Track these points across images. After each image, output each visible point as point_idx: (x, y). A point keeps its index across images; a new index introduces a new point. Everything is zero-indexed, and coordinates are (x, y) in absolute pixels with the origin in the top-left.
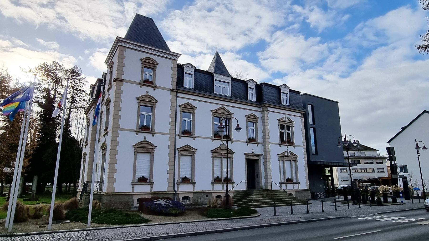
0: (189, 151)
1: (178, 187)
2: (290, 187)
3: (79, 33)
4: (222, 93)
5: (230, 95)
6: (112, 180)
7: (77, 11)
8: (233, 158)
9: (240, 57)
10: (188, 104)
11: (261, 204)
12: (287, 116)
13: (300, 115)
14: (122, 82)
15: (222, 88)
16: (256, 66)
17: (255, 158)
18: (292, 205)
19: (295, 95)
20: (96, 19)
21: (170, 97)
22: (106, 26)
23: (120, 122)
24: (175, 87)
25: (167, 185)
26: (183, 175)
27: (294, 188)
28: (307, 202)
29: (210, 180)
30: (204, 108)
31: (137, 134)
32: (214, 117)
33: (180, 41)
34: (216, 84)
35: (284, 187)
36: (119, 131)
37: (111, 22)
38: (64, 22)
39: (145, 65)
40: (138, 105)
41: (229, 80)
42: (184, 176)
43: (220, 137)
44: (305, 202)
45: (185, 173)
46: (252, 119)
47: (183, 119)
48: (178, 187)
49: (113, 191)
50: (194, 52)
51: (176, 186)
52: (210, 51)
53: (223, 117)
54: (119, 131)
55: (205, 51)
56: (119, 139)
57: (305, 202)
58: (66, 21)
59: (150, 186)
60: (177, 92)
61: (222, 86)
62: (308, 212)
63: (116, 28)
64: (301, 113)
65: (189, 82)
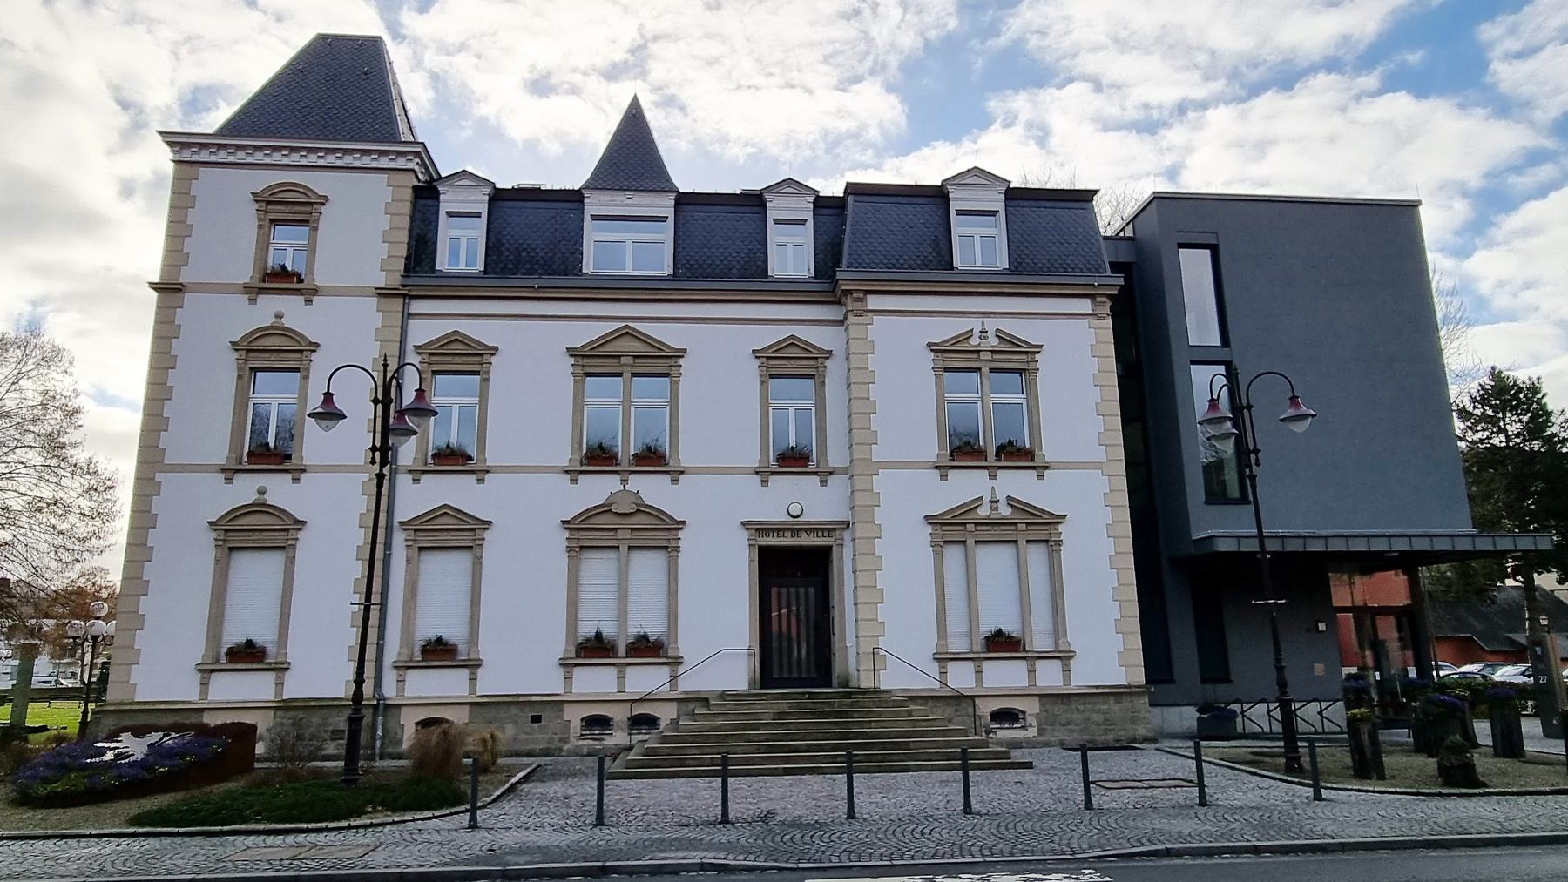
0: (456, 532)
1: (401, 681)
2: (1004, 675)
3: (724, 140)
4: (629, 270)
5: (1002, 262)
7: (712, 62)
8: (1059, 543)
9: (1370, 81)
10: (456, 338)
11: (681, 763)
12: (992, 325)
13: (1085, 306)
14: (179, 295)
15: (977, 238)
16: (1462, 106)
17: (805, 540)
18: (725, 776)
19: (1047, 213)
20: (771, 74)
21: (377, 319)
22: (810, 92)
24: (396, 280)
26: (427, 630)
27: (979, 680)
28: (725, 762)
29: (558, 645)
30: (532, 346)
31: (574, 481)
32: (947, 370)
33: (1085, 78)
34: (959, 227)
35: (961, 678)
36: (159, 477)
37: (824, 68)
38: (676, 111)
39: (272, 216)
40: (239, 369)
41: (664, 206)
42: (432, 636)
43: (980, 453)
44: (712, 762)
45: (440, 618)
46: (788, 363)
48: (401, 681)
49: (126, 698)
50: (1146, 106)
51: (390, 677)
52: (1218, 86)
54: (159, 477)
55: (1199, 93)
57: (712, 762)
58: (683, 109)
59: (465, 673)
60: (404, 296)
61: (629, 237)
63: (842, 87)
64: (1092, 297)
65: (461, 245)
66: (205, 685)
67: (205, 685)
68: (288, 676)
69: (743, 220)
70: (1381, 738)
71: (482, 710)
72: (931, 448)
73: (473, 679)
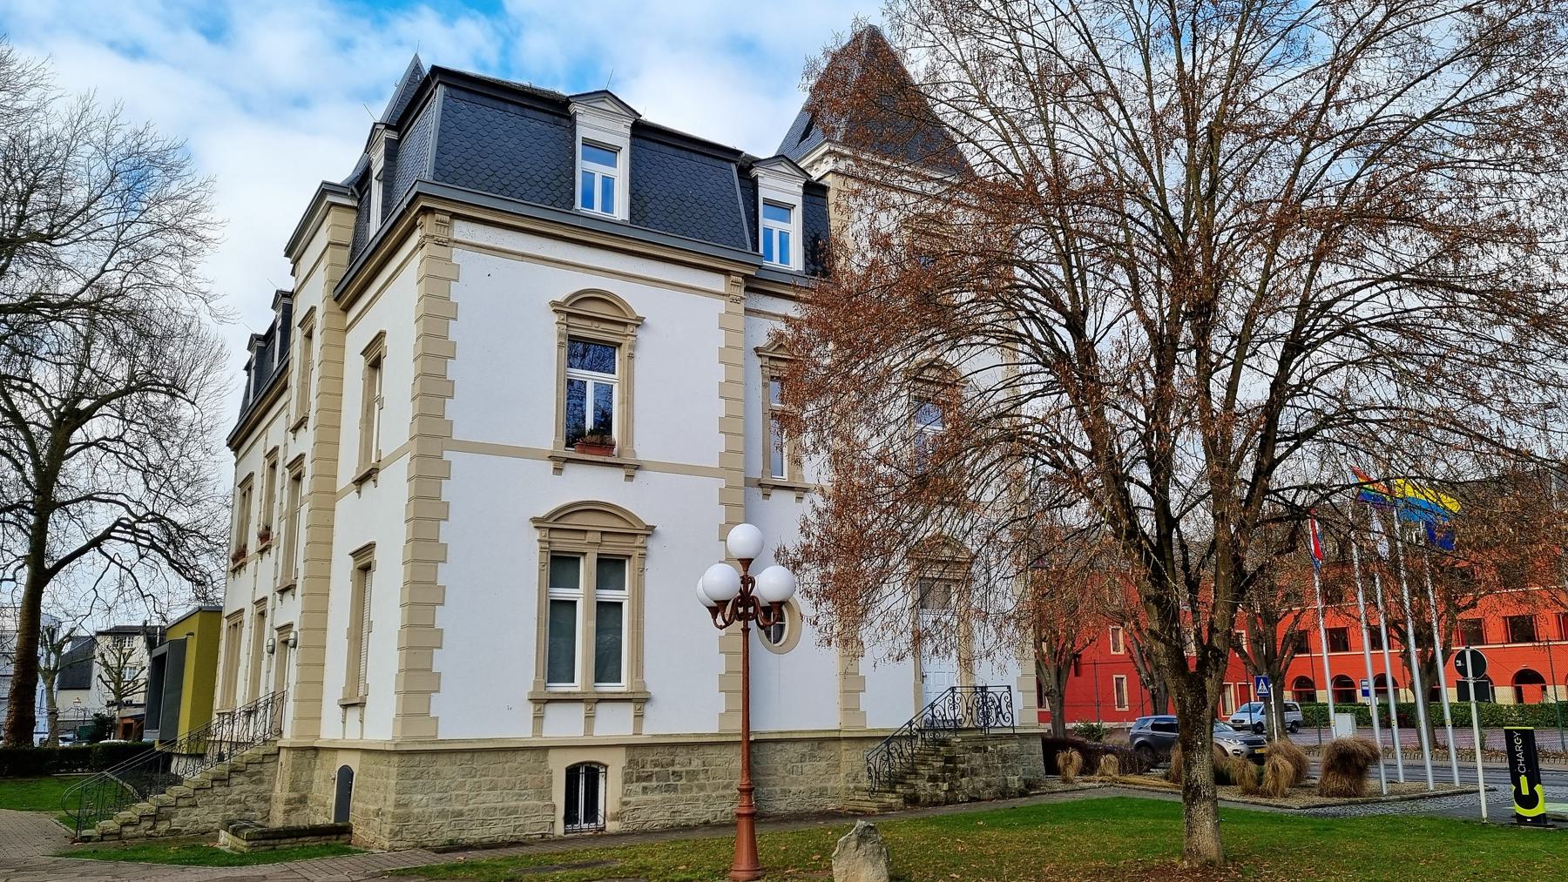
6: (419, 679)
13: (718, 283)
23: (452, 410)
25: (719, 703)
27: (589, 727)
31: (558, 470)
36: (447, 455)
47: (578, 374)
53: (593, 338)
54: (447, 455)
56: (448, 491)
62: (756, 817)
66: (538, 718)
67: (538, 718)
68: (649, 710)
69: (538, 124)
70: (1541, 766)
71: (406, 758)
72: (547, 432)
73: (639, 716)
